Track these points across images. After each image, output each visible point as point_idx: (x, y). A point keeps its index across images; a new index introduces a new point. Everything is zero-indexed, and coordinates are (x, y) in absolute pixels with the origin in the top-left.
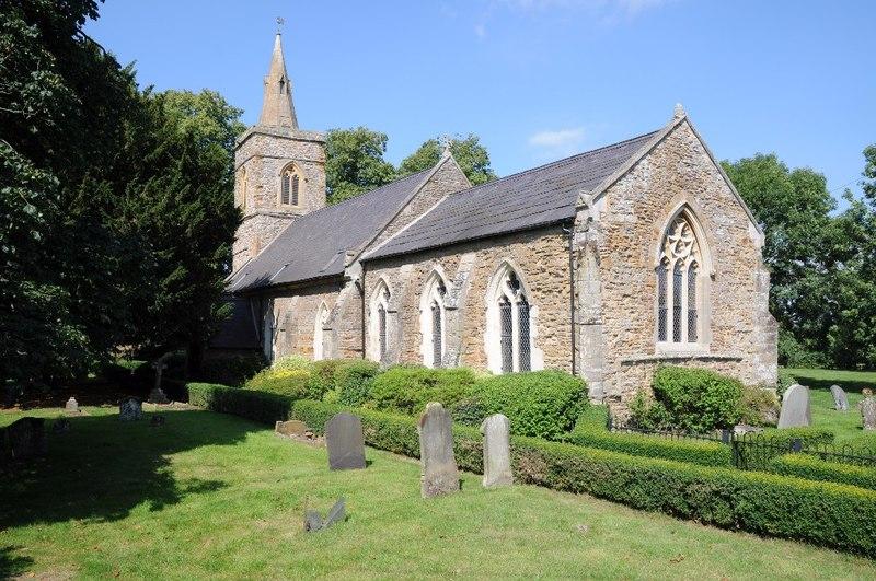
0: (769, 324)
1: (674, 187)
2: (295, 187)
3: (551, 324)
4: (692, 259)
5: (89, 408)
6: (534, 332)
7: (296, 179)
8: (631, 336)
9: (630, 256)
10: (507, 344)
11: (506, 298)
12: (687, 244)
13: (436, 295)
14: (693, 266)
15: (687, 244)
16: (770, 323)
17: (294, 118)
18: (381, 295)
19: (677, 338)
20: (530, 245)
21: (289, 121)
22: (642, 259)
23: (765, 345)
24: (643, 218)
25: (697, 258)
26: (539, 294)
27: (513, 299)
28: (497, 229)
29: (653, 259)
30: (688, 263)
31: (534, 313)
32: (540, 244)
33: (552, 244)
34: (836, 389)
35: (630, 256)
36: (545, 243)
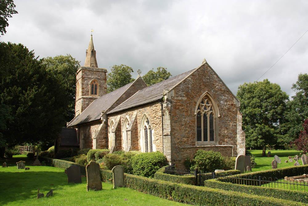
0: (242, 134)
1: (202, 87)
2: (96, 89)
3: (158, 135)
4: (211, 111)
5: (267, 171)
6: (153, 139)
7: (96, 86)
8: (185, 139)
9: (184, 111)
10: (146, 143)
11: (146, 127)
12: (209, 107)
13: (146, 124)
14: (212, 114)
15: (209, 107)
16: (242, 134)
17: (96, 64)
18: (127, 125)
19: (206, 139)
20: (151, 108)
21: (94, 65)
22: (189, 112)
23: (241, 142)
24: (189, 98)
25: (213, 112)
26: (154, 125)
27: (147, 126)
28: (142, 103)
29: (194, 112)
30: (209, 113)
31: (153, 132)
32: (154, 107)
33: (157, 108)
34: (276, 156)
35: (184, 111)
36: (155, 108)
